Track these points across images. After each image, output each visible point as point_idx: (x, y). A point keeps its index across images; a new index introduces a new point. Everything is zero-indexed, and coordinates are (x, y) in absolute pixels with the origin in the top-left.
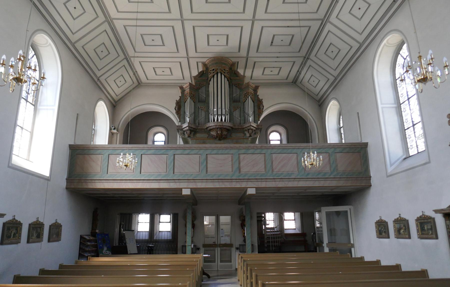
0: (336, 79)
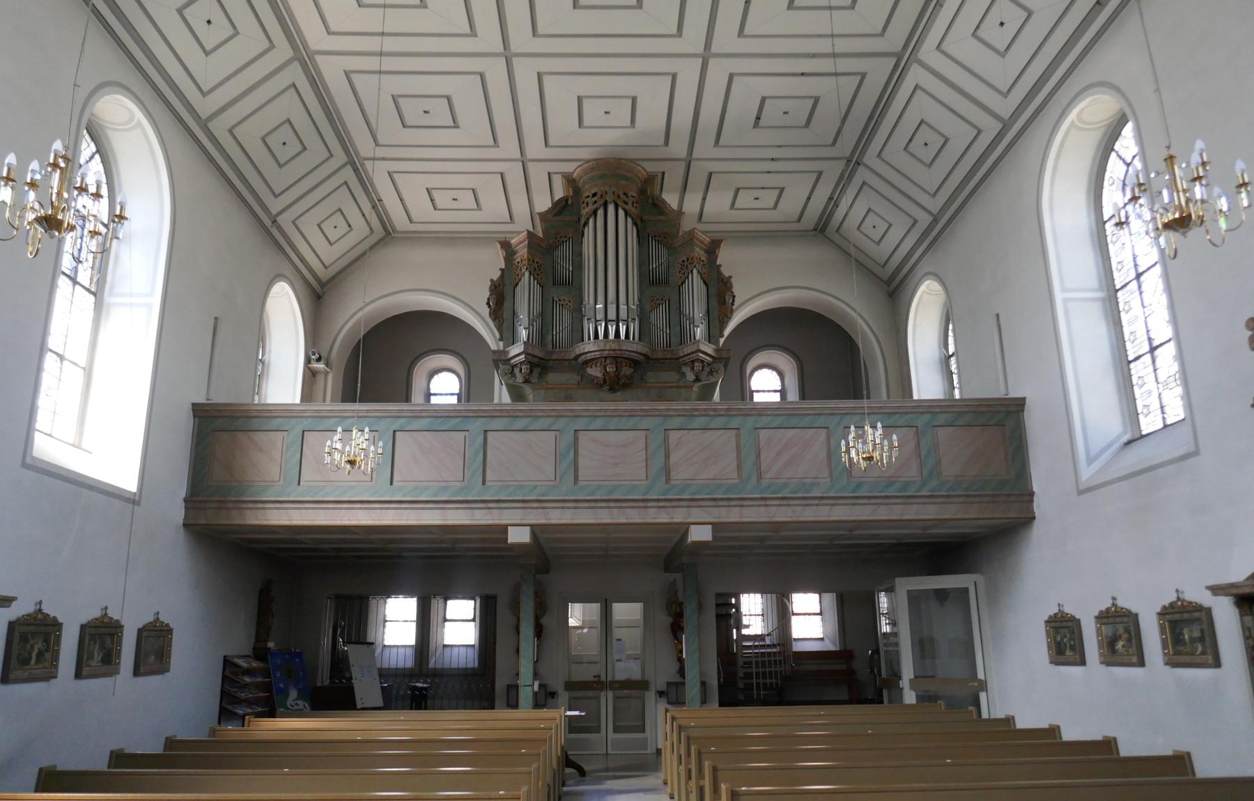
0: (935, 220)
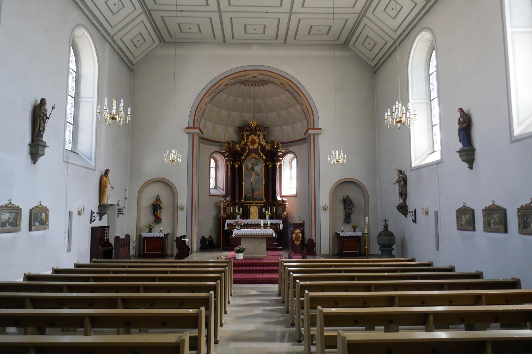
0: (395, 42)
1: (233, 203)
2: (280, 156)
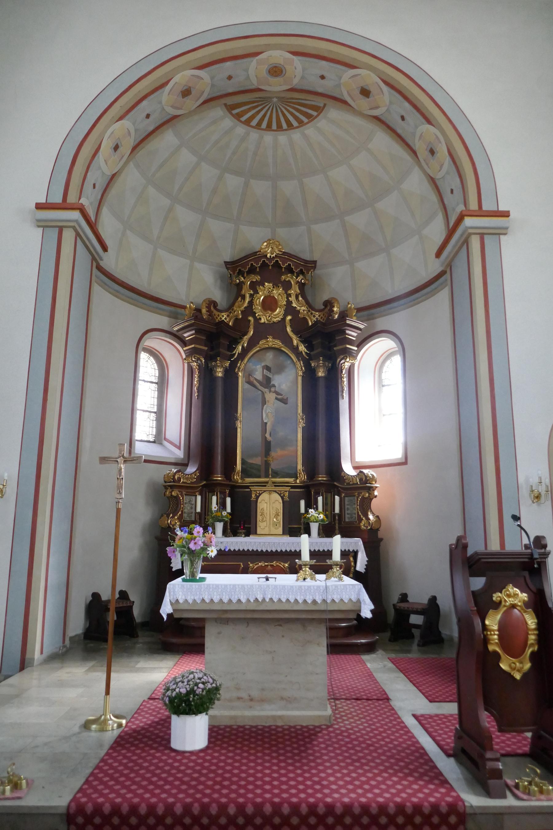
1: (206, 485)
2: (351, 342)
